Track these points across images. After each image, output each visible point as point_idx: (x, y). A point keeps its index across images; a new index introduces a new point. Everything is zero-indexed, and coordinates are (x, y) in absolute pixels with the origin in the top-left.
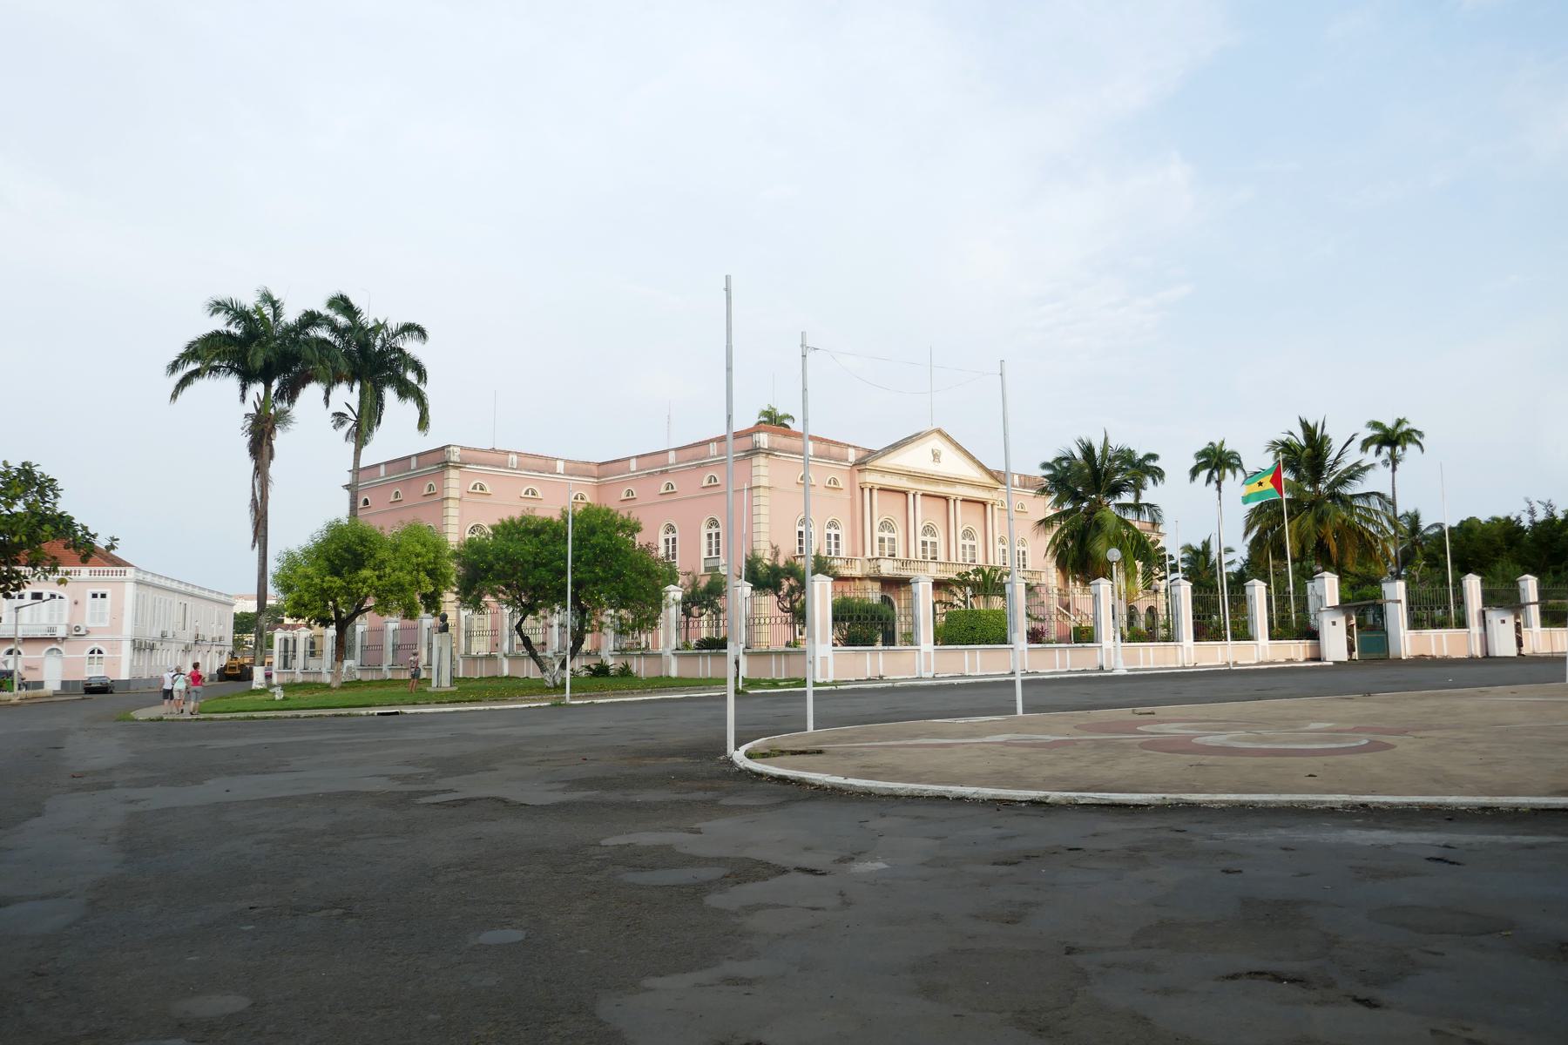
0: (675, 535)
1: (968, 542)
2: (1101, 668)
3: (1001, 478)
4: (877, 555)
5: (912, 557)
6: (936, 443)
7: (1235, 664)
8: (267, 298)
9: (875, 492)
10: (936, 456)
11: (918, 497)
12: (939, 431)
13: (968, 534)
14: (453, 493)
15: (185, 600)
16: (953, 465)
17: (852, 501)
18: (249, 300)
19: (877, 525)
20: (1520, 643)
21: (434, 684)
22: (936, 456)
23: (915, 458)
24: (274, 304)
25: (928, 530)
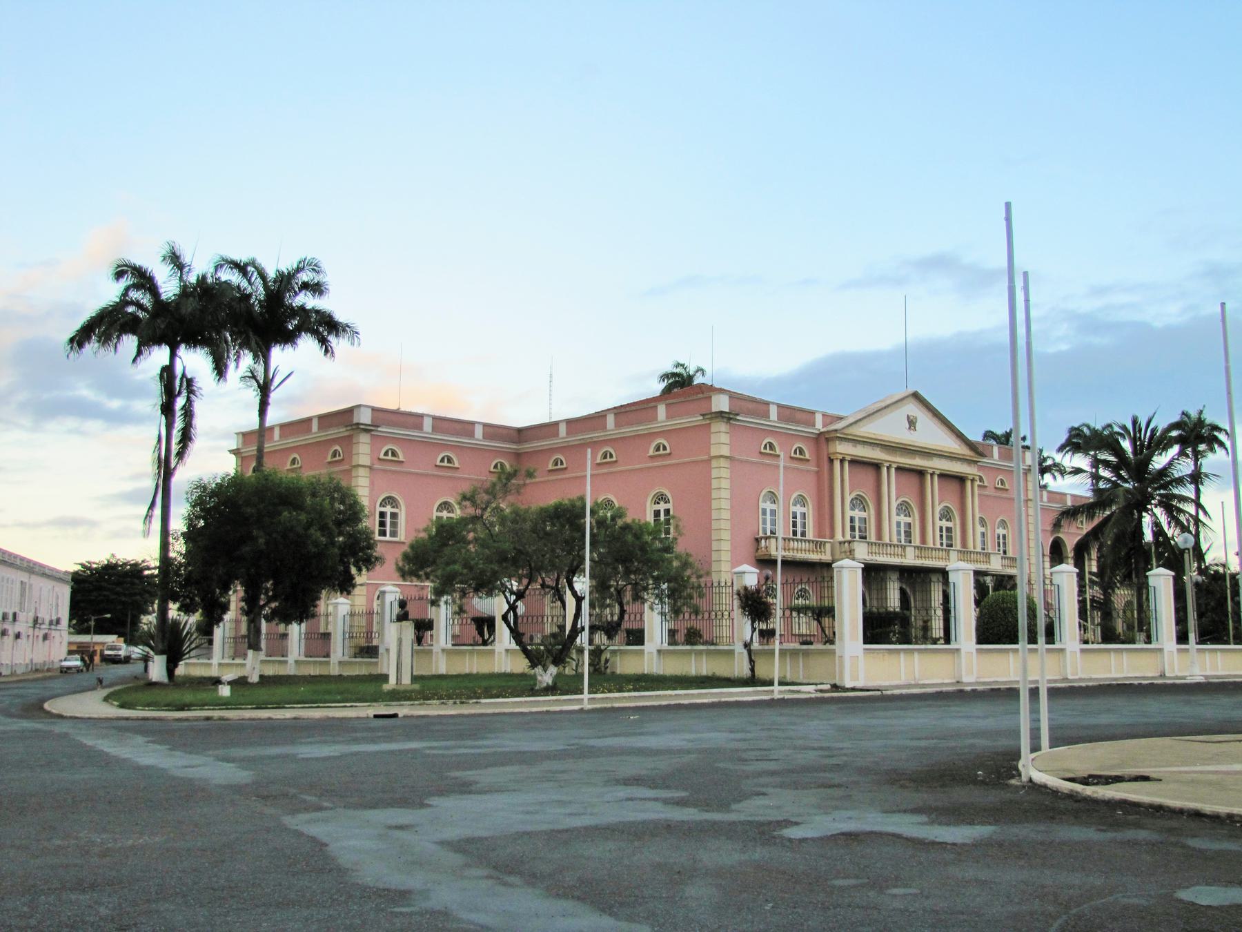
0: (732, 522)
1: (945, 524)
2: (1163, 676)
3: (981, 449)
4: (848, 537)
5: (886, 540)
6: (913, 409)
7: (1065, 680)
8: (678, 365)
9: (846, 465)
10: (912, 423)
11: (893, 470)
12: (916, 396)
13: (947, 514)
14: (364, 460)
15: (24, 577)
16: (930, 435)
17: (818, 474)
18: (670, 369)
19: (937, 516)
20: (752, 670)
21: (392, 680)
22: (912, 423)
23: (891, 428)
24: (683, 365)
25: (947, 514)
